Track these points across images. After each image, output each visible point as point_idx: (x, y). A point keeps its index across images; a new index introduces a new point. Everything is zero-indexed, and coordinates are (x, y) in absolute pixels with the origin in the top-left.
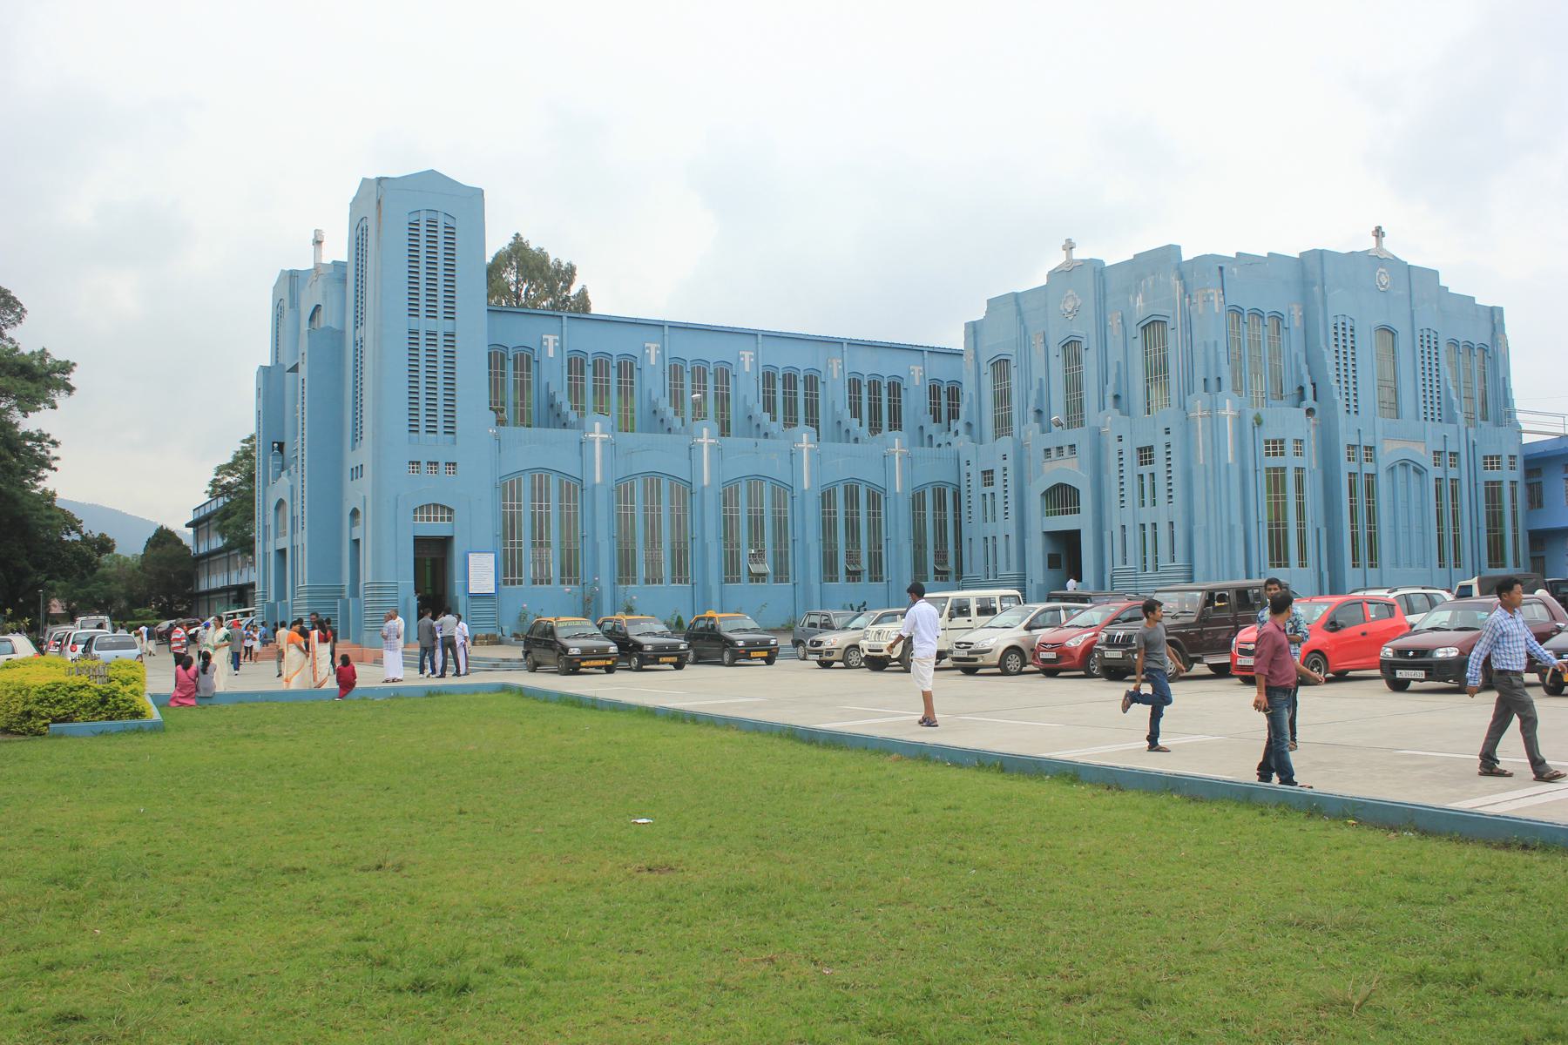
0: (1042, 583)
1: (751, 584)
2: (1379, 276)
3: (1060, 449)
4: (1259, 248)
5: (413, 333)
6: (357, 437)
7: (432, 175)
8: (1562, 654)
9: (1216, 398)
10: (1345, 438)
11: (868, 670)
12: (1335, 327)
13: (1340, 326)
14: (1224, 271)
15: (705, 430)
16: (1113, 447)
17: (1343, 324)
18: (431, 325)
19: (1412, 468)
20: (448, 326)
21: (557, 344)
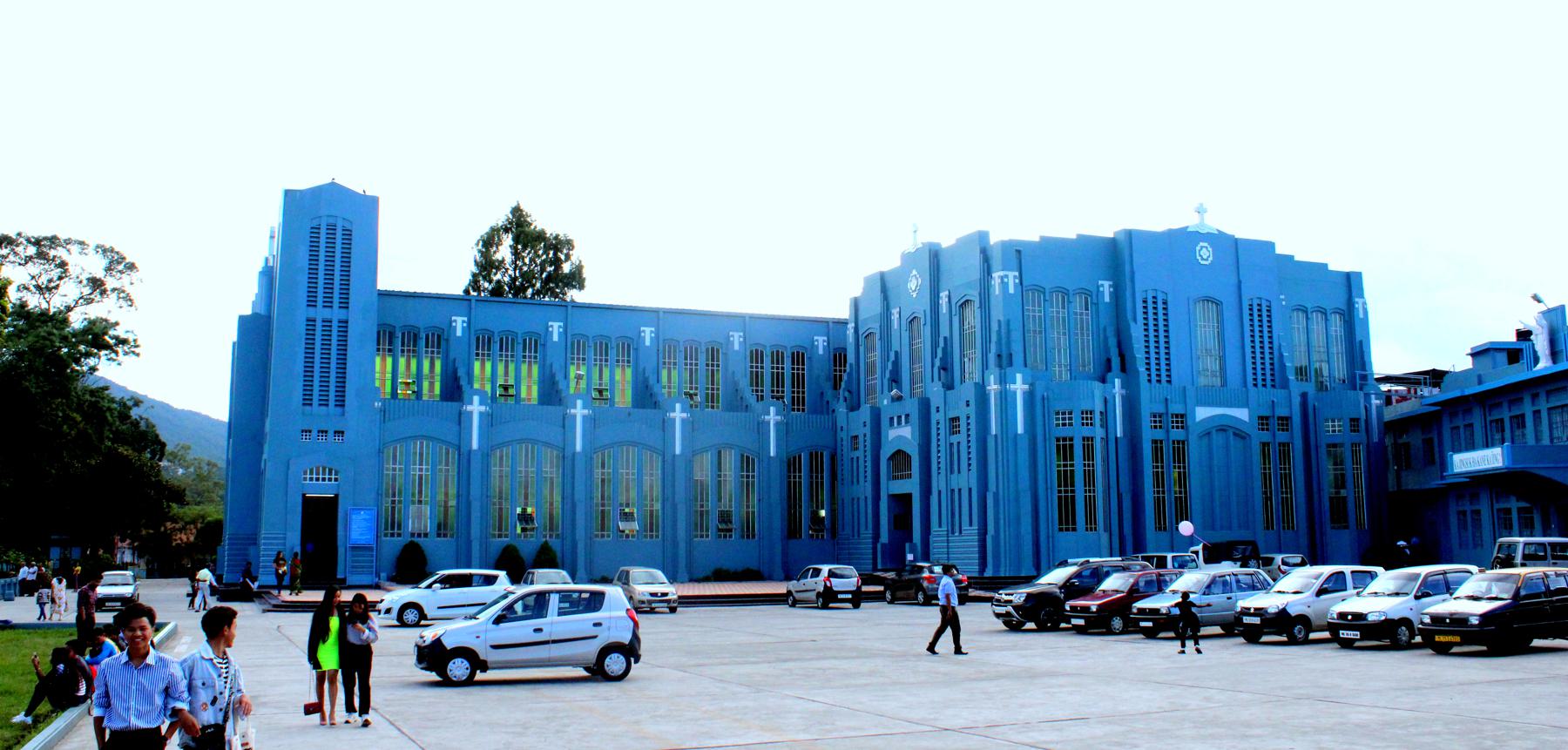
3: (899, 417)
4: (1067, 230)
5: (311, 321)
7: (333, 184)
9: (1005, 373)
10: (1147, 408)
12: (1144, 301)
13: (1150, 300)
16: (935, 417)
17: (1154, 297)
18: (327, 313)
19: (1231, 434)
20: (342, 314)
21: (465, 325)
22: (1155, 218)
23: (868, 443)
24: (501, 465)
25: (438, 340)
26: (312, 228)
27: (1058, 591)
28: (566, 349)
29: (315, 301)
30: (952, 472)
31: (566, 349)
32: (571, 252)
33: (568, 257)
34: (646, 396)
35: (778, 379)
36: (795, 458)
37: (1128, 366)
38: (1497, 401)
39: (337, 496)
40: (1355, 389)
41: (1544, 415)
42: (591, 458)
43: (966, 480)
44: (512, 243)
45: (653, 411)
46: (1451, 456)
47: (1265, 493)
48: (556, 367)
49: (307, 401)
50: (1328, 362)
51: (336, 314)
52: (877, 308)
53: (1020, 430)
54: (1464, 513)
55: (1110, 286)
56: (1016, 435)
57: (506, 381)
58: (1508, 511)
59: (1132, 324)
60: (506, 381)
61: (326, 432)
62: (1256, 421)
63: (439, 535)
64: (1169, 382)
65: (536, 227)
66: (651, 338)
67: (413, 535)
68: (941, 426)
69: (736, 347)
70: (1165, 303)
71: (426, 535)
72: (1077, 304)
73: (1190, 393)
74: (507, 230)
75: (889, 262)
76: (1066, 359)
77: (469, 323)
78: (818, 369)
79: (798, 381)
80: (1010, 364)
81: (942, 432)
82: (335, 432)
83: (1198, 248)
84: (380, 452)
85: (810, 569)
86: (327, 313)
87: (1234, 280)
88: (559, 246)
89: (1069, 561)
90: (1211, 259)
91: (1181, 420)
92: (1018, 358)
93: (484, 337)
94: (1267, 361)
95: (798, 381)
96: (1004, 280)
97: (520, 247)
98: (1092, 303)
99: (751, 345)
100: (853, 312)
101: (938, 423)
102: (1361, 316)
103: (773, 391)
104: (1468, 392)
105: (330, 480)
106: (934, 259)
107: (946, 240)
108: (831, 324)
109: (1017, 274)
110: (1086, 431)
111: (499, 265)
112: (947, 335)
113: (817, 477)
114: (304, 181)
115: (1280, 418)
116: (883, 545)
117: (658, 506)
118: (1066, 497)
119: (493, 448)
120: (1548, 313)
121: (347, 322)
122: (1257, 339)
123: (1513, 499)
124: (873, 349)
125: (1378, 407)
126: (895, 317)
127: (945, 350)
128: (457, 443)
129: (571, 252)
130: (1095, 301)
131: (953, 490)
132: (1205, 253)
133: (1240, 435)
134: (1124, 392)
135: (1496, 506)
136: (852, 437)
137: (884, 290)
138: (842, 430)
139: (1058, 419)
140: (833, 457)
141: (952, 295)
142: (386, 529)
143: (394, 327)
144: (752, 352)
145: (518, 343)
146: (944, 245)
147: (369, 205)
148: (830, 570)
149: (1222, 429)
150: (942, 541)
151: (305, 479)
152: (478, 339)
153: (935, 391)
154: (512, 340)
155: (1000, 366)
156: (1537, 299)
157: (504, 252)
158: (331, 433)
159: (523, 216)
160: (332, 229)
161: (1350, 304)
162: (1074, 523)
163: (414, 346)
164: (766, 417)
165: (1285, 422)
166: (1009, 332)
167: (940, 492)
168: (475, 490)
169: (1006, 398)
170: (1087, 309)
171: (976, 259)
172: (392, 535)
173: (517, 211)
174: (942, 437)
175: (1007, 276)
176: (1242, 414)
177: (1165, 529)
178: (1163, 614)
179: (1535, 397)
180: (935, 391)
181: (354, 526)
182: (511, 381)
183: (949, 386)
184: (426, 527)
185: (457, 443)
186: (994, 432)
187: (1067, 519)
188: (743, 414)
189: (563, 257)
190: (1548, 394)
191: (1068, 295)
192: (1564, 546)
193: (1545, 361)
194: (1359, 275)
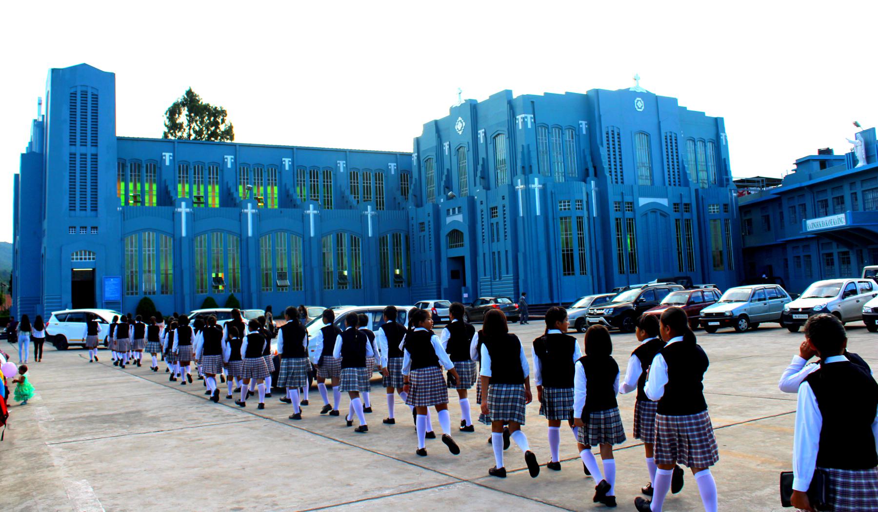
0: (447, 287)
1: (162, 295)
2: (637, 103)
3: (454, 209)
4: (560, 90)
5: (73, 155)
6: (45, 218)
8: (758, 324)
9: (528, 178)
10: (613, 197)
11: (706, 332)
13: (610, 133)
14: (535, 104)
15: (369, 207)
16: (479, 207)
18: (83, 150)
19: (659, 214)
20: (93, 150)
22: (612, 85)
23: (432, 226)
24: (201, 246)
25: (154, 168)
26: (71, 94)
27: (632, 305)
28: (236, 172)
29: (75, 139)
30: (493, 241)
31: (236, 172)
32: (225, 118)
33: (223, 121)
34: (287, 200)
35: (367, 190)
36: (383, 238)
37: (598, 173)
38: (840, 185)
39: (94, 270)
40: (723, 186)
41: (860, 196)
42: (258, 240)
43: (504, 245)
44: (187, 113)
45: (293, 209)
46: (805, 221)
47: (678, 249)
48: (230, 184)
49: (72, 208)
50: (707, 171)
51: (89, 150)
52: (433, 142)
53: (538, 213)
54: (799, 257)
55: (586, 124)
56: (536, 216)
57: (199, 193)
58: (831, 255)
59: (600, 147)
60: (199, 193)
61: (86, 228)
62: (672, 207)
63: (162, 293)
64: (622, 183)
65: (202, 103)
66: (289, 165)
67: (145, 293)
68: (485, 213)
69: (342, 170)
70: (619, 134)
71: (154, 293)
72: (567, 135)
73: (635, 189)
74: (184, 105)
75: (442, 113)
76: (561, 169)
77: (174, 156)
78: (390, 185)
79: (379, 191)
80: (531, 172)
81: (485, 216)
82: (92, 228)
83: (636, 101)
84: (122, 240)
85: (420, 303)
86: (83, 150)
87: (656, 121)
88: (217, 114)
89: (631, 286)
90: (643, 108)
91: (631, 205)
92: (535, 169)
93: (183, 166)
94: (676, 170)
95: (379, 191)
96: (524, 120)
97: (193, 115)
98: (576, 134)
99: (350, 169)
100: (416, 147)
101: (482, 211)
102: (724, 143)
103: (364, 198)
104: (805, 184)
105: (89, 259)
106: (473, 110)
107: (481, 97)
108: (398, 156)
109: (532, 116)
110: (579, 213)
111: (180, 127)
112: (485, 156)
113: (397, 249)
114: (65, 62)
115: (686, 205)
116: (445, 289)
117: (301, 270)
118: (568, 254)
119: (195, 236)
120: (863, 133)
121: (96, 155)
122: (670, 157)
123: (834, 245)
124: (431, 169)
125: (735, 198)
126: (446, 147)
127: (483, 166)
128: (172, 233)
129: (225, 118)
130: (577, 134)
131: (494, 253)
132: (640, 104)
133: (664, 215)
134: (597, 189)
135: (822, 252)
136: (490, 208)
137: (438, 131)
138: (412, 219)
139: (561, 206)
140: (407, 238)
141: (487, 132)
142: (128, 290)
143: (125, 160)
144: (351, 173)
145: (205, 169)
146: (479, 102)
147: (109, 79)
148: (435, 303)
149: (654, 211)
150: (487, 285)
151: (73, 259)
152: (180, 167)
153: (478, 192)
154: (202, 167)
155: (524, 173)
156: (857, 125)
157: (183, 118)
158: (89, 228)
159: (193, 96)
160: (84, 94)
161: (718, 136)
162: (573, 270)
163: (139, 172)
164: (366, 212)
165: (687, 206)
166: (529, 152)
167: (484, 254)
168: (185, 264)
169: (528, 193)
170: (573, 138)
171: (505, 107)
172: (132, 294)
173: (190, 93)
174: (485, 220)
175: (526, 117)
176: (664, 202)
177: (624, 273)
178: (727, 316)
179: (853, 184)
180: (478, 192)
181: (107, 289)
182: (202, 194)
183: (487, 188)
184: (154, 288)
185: (172, 233)
186: (521, 215)
187: (568, 268)
188: (349, 210)
189: (220, 121)
190: (862, 181)
191: (562, 129)
192: (876, 271)
193: (862, 162)
194: (722, 119)
